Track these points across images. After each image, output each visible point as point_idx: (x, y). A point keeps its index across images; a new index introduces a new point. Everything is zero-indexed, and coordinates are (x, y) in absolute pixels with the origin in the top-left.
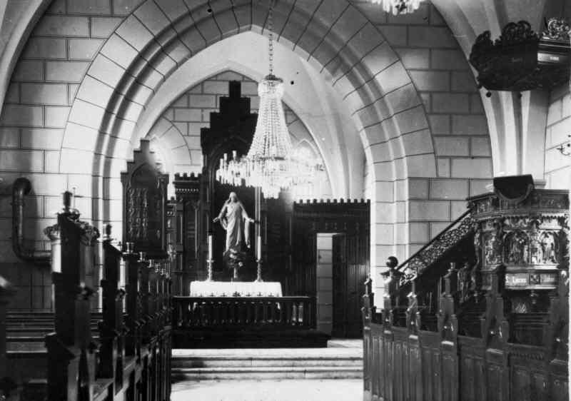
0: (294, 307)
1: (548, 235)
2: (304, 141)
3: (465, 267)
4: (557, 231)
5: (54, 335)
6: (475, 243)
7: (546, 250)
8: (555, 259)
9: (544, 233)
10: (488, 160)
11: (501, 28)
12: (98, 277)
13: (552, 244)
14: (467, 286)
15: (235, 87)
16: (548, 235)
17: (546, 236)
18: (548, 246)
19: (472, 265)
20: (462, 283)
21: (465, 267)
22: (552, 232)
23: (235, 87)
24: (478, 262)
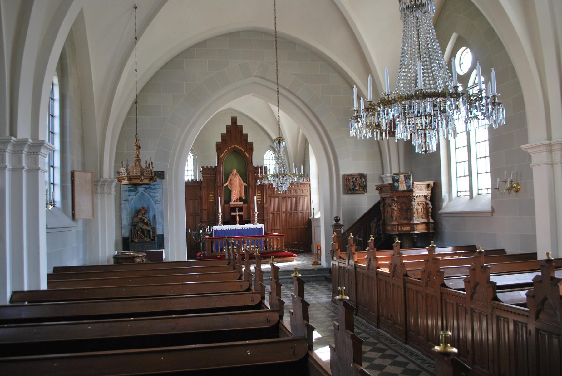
0: (210, 201)
1: (420, 204)
2: (150, 231)
3: (375, 220)
4: (423, 202)
5: (247, 156)
6: (381, 208)
7: (419, 212)
8: (423, 216)
9: (417, 203)
10: (49, 227)
11: (308, 141)
12: (157, 238)
13: (421, 209)
14: (376, 230)
15: (234, 120)
16: (420, 204)
17: (419, 205)
18: (420, 211)
19: (379, 220)
20: (374, 229)
21: (375, 220)
22: (421, 203)
23: (234, 120)
24: (383, 218)
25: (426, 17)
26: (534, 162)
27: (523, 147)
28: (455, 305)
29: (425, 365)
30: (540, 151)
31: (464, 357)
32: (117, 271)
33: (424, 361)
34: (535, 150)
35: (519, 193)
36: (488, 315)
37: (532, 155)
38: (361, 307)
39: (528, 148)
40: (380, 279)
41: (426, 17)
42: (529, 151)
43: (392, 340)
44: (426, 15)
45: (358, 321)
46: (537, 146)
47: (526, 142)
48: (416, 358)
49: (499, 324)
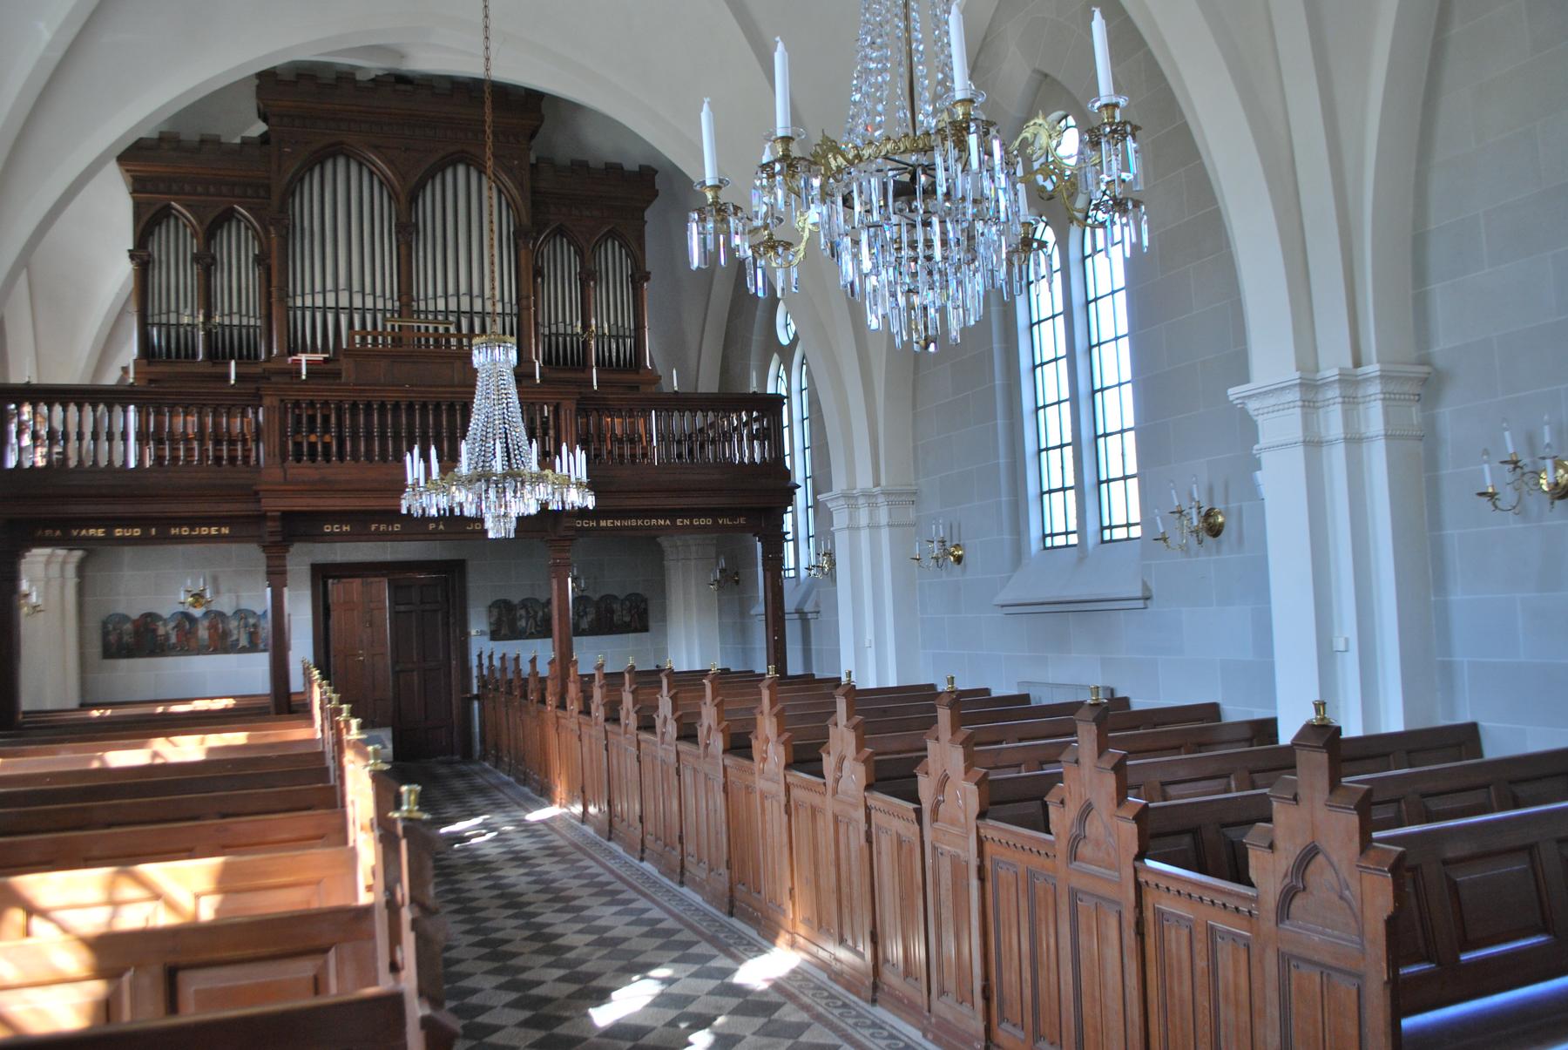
25: (884, 81)
26: (1264, 440)
27: (1234, 392)
28: (1200, 935)
29: (862, 1031)
30: (1286, 406)
31: (1014, 1025)
32: (63, 835)
33: (894, 1041)
34: (1271, 401)
35: (1222, 536)
36: (1124, 912)
37: (1260, 420)
38: (743, 888)
39: (1249, 397)
40: (1160, 915)
41: (884, 81)
42: (1252, 406)
43: (863, 1012)
44: (918, 51)
45: (717, 924)
46: (1276, 389)
47: (1245, 378)
48: (872, 1035)
49: (480, 717)
